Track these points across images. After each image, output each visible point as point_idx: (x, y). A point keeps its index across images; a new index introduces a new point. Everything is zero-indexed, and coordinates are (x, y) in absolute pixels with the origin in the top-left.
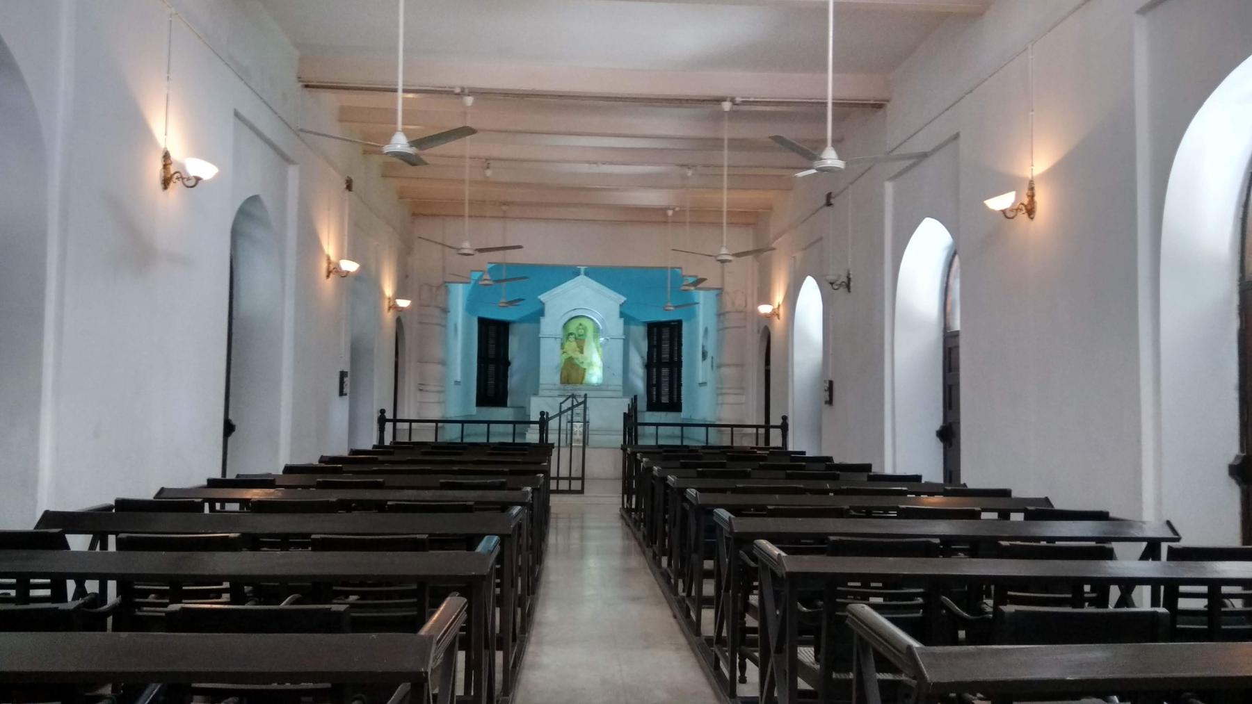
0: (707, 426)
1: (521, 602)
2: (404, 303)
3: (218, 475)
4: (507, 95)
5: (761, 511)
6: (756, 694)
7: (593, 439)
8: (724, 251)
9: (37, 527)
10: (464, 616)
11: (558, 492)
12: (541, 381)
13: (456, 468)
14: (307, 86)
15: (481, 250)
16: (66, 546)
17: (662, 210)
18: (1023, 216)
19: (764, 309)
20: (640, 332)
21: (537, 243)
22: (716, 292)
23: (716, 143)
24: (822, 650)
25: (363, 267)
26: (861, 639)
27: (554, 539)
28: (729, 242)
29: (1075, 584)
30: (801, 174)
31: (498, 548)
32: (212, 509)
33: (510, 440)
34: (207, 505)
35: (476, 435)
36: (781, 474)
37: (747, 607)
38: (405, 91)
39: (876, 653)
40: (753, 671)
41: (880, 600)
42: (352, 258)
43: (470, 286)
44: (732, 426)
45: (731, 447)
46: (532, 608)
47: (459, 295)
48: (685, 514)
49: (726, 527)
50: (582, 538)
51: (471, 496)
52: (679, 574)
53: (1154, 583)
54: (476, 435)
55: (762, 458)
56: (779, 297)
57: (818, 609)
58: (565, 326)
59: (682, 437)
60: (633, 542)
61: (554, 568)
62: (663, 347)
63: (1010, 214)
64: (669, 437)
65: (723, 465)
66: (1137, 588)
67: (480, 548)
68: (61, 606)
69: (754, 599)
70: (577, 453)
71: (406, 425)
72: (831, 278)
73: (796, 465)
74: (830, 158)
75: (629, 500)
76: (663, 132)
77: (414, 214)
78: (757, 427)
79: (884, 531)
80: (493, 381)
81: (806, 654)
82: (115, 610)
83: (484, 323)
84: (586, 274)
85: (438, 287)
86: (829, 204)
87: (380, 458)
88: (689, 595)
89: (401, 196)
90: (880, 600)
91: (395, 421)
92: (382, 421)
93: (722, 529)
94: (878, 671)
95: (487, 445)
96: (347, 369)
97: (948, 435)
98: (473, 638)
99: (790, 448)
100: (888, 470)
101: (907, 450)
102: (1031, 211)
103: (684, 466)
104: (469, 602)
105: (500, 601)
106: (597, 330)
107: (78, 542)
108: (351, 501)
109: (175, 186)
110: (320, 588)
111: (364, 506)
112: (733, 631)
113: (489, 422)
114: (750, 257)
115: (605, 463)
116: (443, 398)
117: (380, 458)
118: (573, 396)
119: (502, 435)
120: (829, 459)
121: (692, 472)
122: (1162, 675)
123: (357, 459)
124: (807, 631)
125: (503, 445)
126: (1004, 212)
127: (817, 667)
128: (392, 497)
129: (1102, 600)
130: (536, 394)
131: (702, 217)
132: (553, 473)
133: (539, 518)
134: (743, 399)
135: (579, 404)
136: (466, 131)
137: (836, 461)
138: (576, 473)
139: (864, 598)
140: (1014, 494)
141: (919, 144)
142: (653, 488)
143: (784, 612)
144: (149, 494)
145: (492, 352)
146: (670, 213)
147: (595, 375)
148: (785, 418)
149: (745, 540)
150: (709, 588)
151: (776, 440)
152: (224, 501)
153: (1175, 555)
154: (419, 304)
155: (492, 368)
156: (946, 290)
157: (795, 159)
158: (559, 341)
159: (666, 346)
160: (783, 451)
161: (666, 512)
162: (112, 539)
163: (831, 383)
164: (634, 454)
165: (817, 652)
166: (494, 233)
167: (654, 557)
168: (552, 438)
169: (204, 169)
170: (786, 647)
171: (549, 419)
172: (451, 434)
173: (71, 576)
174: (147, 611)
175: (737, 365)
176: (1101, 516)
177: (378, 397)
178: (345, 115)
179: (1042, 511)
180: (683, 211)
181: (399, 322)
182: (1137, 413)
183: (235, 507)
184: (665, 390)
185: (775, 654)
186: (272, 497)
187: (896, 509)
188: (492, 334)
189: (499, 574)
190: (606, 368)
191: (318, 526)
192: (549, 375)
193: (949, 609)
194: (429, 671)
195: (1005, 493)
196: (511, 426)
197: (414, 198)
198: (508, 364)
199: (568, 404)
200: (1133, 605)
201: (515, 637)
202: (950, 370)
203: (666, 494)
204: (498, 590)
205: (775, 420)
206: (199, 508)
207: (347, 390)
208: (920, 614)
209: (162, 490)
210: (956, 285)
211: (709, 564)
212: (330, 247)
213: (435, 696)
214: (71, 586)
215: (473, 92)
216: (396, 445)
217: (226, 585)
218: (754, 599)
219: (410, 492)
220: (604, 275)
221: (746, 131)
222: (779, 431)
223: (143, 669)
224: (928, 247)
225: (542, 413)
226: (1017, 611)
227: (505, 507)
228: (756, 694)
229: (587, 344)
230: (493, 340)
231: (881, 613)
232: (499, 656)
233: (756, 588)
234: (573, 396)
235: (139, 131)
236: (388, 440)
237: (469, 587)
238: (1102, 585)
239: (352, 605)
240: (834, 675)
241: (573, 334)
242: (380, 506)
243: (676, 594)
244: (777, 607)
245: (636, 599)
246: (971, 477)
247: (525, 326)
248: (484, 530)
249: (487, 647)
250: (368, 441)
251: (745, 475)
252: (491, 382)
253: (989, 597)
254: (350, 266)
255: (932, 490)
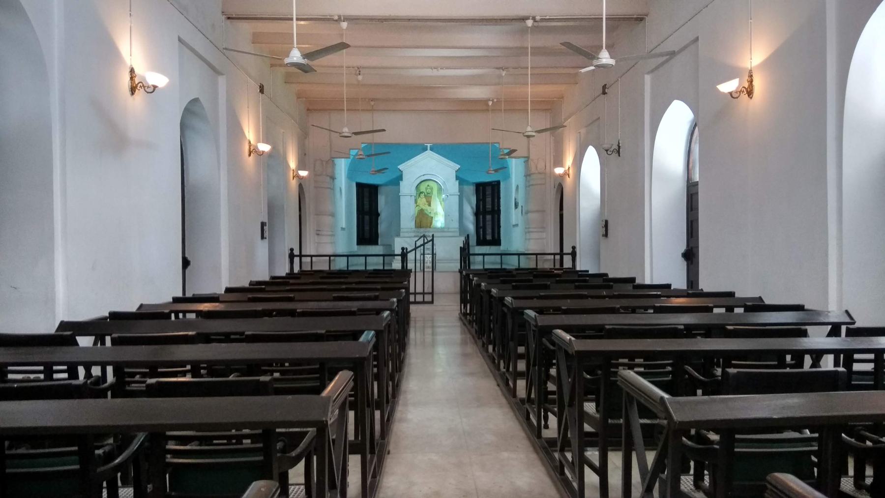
0: (519, 255)
1: (392, 378)
2: (303, 173)
3: (179, 294)
4: (371, 19)
5: (558, 311)
6: (555, 435)
7: (439, 266)
8: (529, 129)
9: (57, 330)
10: (352, 384)
11: (415, 303)
12: (402, 226)
13: (344, 287)
14: (229, 18)
15: (356, 134)
16: (77, 344)
17: (485, 102)
18: (744, 96)
19: (559, 171)
20: (470, 190)
21: (396, 127)
22: (523, 160)
23: (521, 51)
24: (602, 401)
25: (273, 148)
26: (628, 393)
27: (414, 335)
28: (533, 123)
29: (780, 355)
30: (583, 70)
31: (374, 340)
32: (177, 317)
33: (381, 268)
34: (173, 315)
35: (358, 264)
36: (572, 286)
37: (548, 377)
38: (297, 19)
39: (640, 405)
40: (553, 420)
41: (642, 369)
42: (266, 141)
43: (350, 160)
44: (537, 254)
45: (536, 269)
46: (399, 381)
47: (342, 166)
48: (504, 315)
49: (533, 323)
50: (433, 334)
51: (354, 306)
52: (501, 357)
53: (836, 352)
54: (356, 265)
55: (558, 275)
56: (569, 161)
57: (597, 375)
58: (417, 187)
59: (501, 264)
60: (469, 336)
61: (414, 355)
62: (487, 200)
63: (735, 95)
64: (492, 263)
65: (531, 281)
66: (825, 356)
67: (362, 339)
68: (74, 382)
69: (553, 371)
70: (428, 277)
71: (309, 259)
72: (606, 146)
73: (583, 280)
74: (605, 58)
75: (465, 307)
76: (483, 44)
77: (308, 110)
78: (554, 254)
79: (643, 322)
80: (368, 228)
81: (590, 407)
82: (112, 387)
83: (360, 187)
84: (431, 150)
85: (327, 162)
86: (604, 93)
87: (291, 281)
88: (508, 370)
89: (299, 96)
90: (642, 369)
91: (301, 256)
92: (292, 256)
93: (530, 324)
94: (641, 418)
95: (365, 272)
96: (266, 220)
97: (690, 256)
98: (359, 401)
99: (578, 269)
100: (648, 281)
101: (661, 266)
102: (750, 93)
103: (504, 282)
104: (356, 375)
105: (377, 377)
106: (440, 189)
107: (85, 341)
108: (273, 310)
109: (140, 93)
110: (253, 367)
111: (281, 313)
112: (539, 393)
113: (366, 256)
114: (548, 133)
115: (448, 282)
116: (334, 239)
117: (291, 281)
118: (424, 236)
119: (375, 264)
120: (606, 275)
121: (509, 286)
122: (841, 414)
123: (275, 281)
124: (590, 391)
125: (376, 272)
126: (731, 93)
127: (598, 416)
128: (300, 307)
129: (800, 364)
130: (398, 235)
131: (513, 105)
132: (412, 290)
133: (402, 322)
134: (544, 235)
135: (428, 242)
136: (343, 46)
137: (611, 276)
138: (428, 289)
139: (631, 367)
140: (736, 295)
141: (671, 45)
142: (482, 297)
143: (574, 380)
144: (133, 308)
145: (367, 207)
146: (490, 103)
147: (439, 221)
148: (574, 248)
149: (546, 331)
150: (522, 366)
151: (567, 263)
152: (184, 312)
153: (852, 333)
154: (315, 174)
155: (367, 218)
156: (689, 153)
157: (581, 59)
158: (413, 198)
159: (489, 200)
160: (573, 271)
161: (491, 314)
162: (108, 339)
163: (606, 222)
164: (468, 275)
165: (597, 406)
166: (365, 121)
167: (483, 346)
168: (411, 266)
169: (159, 80)
170: (576, 402)
171: (407, 253)
172: (340, 264)
173: (81, 364)
174: (134, 387)
175: (537, 211)
176: (799, 308)
177: (289, 239)
178: (256, 38)
179: (757, 306)
180: (499, 101)
181: (300, 186)
182: (825, 232)
183: (193, 316)
184: (489, 230)
185: (568, 407)
186: (218, 309)
187: (654, 308)
188: (366, 194)
189: (376, 358)
190: (447, 216)
191: (250, 327)
192: (407, 221)
193: (691, 375)
194: (329, 423)
195: (731, 295)
196: (381, 258)
197: (308, 100)
198: (378, 215)
199: (420, 242)
200: (820, 367)
201: (388, 400)
202: (692, 210)
203: (491, 302)
204: (375, 370)
205: (567, 249)
206: (168, 316)
207: (266, 234)
208: (670, 378)
209: (141, 306)
210: (696, 148)
211: (521, 350)
212: (250, 133)
213: (334, 440)
214: (81, 371)
215: (348, 19)
216: (302, 273)
217: (189, 367)
218: (553, 371)
219: (312, 303)
220: (444, 150)
221: (542, 41)
222: (570, 257)
223: (132, 423)
224: (677, 119)
225: (403, 249)
226: (738, 372)
227: (379, 312)
228: (555, 435)
229: (432, 198)
230: (367, 198)
231: (645, 378)
232: (377, 414)
233: (554, 364)
234: (424, 236)
235: (111, 53)
236: (296, 269)
237: (357, 365)
238: (799, 355)
239: (276, 380)
240: (610, 421)
241: (423, 192)
242: (292, 313)
243: (499, 369)
244: (569, 377)
245: (471, 374)
246: (705, 285)
247: (390, 188)
248: (363, 328)
249: (368, 406)
250: (283, 270)
251: (546, 287)
252: (367, 228)
253: (719, 366)
254: (265, 147)
255: (679, 294)
